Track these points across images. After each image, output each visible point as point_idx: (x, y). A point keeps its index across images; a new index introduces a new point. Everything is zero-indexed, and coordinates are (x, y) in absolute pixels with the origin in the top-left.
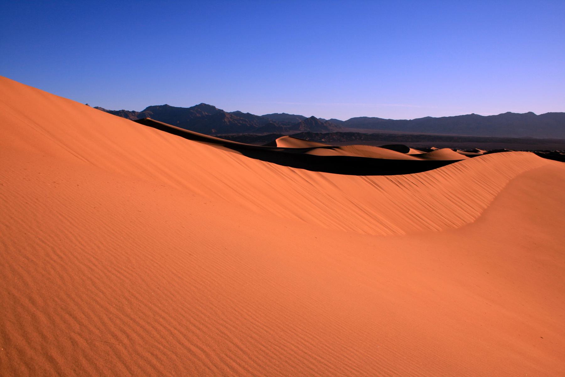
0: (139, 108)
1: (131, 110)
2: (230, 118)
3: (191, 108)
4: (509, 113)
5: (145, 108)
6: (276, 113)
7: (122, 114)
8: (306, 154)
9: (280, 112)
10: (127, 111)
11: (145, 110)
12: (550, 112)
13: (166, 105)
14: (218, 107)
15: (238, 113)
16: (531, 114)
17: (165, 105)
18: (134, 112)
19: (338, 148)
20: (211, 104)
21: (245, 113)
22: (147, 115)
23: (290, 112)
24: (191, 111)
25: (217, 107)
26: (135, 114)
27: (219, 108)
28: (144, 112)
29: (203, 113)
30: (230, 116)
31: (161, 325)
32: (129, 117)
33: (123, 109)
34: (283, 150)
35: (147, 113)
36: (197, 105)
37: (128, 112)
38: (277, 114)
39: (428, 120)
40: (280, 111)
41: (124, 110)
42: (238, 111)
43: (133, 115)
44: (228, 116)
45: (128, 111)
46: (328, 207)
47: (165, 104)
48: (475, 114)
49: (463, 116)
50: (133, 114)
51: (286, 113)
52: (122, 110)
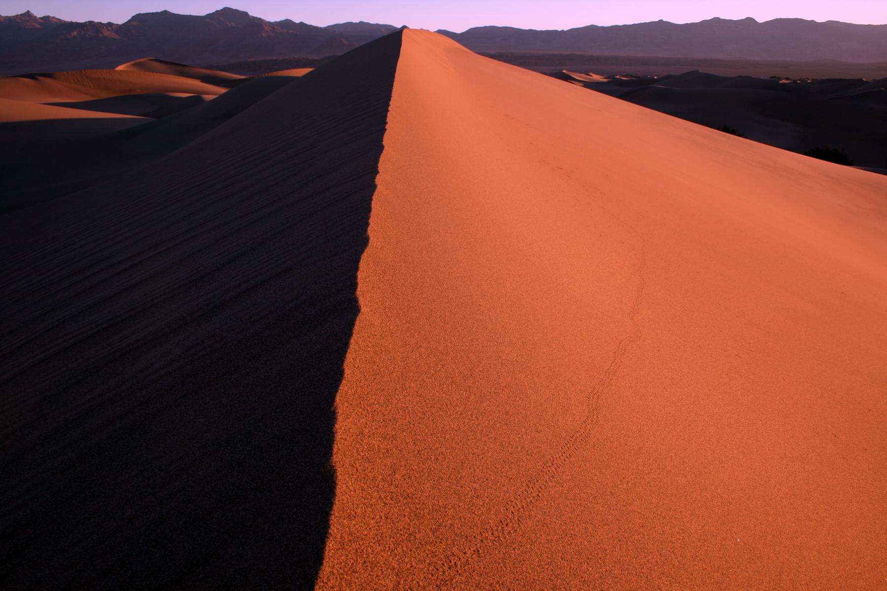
0: (460, 28)
1: (105, 21)
2: (271, 31)
3: (209, 16)
4: (716, 20)
6: (350, 21)
7: (89, 28)
9: (356, 20)
10: (98, 23)
13: (166, 11)
14: (253, 13)
15: (288, 23)
16: (750, 21)
17: (163, 11)
18: (110, 24)
19: (49, 76)
20: (241, 8)
21: (272, 21)
23: (373, 21)
24: (207, 20)
25: (251, 14)
27: (255, 15)
29: (228, 24)
30: (270, 28)
33: (91, 20)
34: (571, 81)
36: (217, 11)
38: (352, 22)
39: (592, 30)
40: (355, 18)
42: (287, 20)
43: (108, 30)
45: (100, 23)
47: (164, 10)
48: (664, 20)
49: (645, 23)
50: (109, 28)
51: (365, 21)
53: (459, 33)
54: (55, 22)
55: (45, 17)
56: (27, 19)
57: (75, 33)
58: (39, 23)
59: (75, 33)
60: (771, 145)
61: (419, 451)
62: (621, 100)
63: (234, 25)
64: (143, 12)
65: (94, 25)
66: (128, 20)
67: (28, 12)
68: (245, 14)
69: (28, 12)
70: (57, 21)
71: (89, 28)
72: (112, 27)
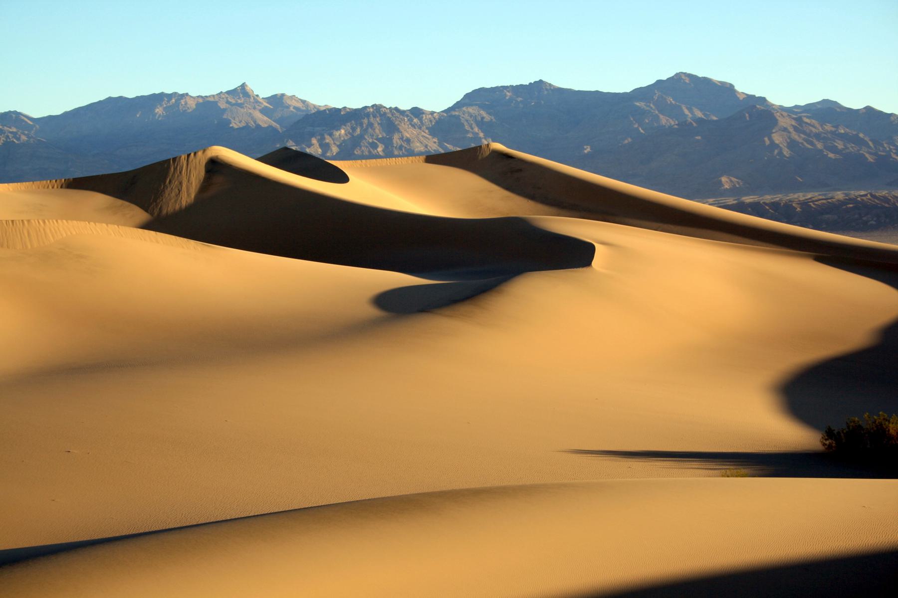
1: (405, 106)
18: (416, 112)
20: (717, 76)
29: (686, 112)
30: (794, 123)
36: (659, 82)
50: (415, 120)
53: (700, 76)
54: (295, 108)
55: (274, 97)
56: (239, 101)
57: (343, 131)
58: (264, 111)
59: (343, 131)
60: (842, 478)
61: (113, 518)
62: (48, 544)
63: (699, 114)
64: (488, 85)
65: (385, 114)
66: (455, 102)
67: (243, 86)
68: (728, 89)
69: (243, 86)
70: (300, 105)
71: (372, 119)
72: (421, 120)
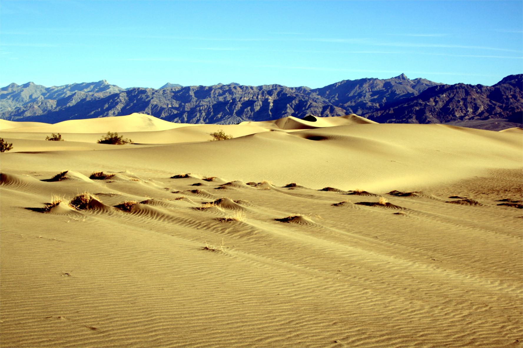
1: (474, 83)
5: (501, 79)
8: (70, 107)
10: (467, 85)
11: (499, 83)
12: (356, 79)
18: (480, 86)
22: (502, 91)
26: (481, 90)
28: (497, 87)
31: (130, 345)
32: (470, 95)
33: (461, 82)
35: (503, 88)
37: (470, 87)
41: (463, 84)
44: (315, 95)
45: (470, 85)
46: (81, 344)
50: (479, 90)
52: (459, 84)
